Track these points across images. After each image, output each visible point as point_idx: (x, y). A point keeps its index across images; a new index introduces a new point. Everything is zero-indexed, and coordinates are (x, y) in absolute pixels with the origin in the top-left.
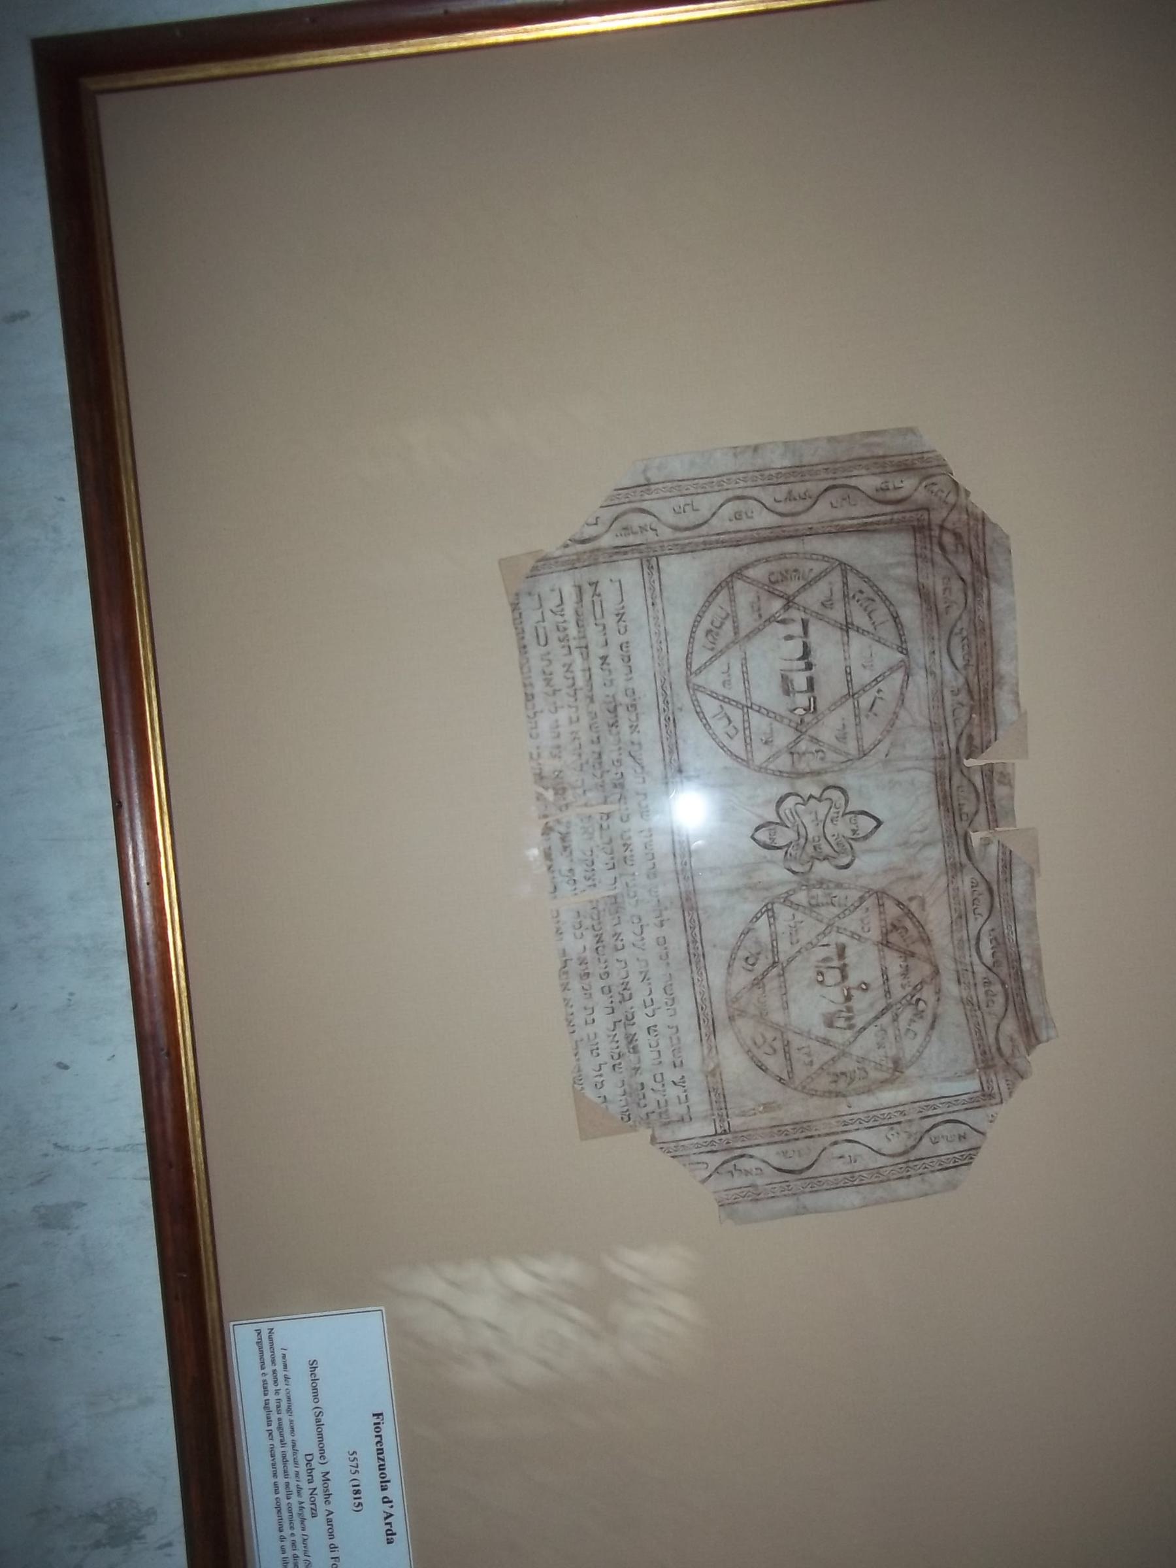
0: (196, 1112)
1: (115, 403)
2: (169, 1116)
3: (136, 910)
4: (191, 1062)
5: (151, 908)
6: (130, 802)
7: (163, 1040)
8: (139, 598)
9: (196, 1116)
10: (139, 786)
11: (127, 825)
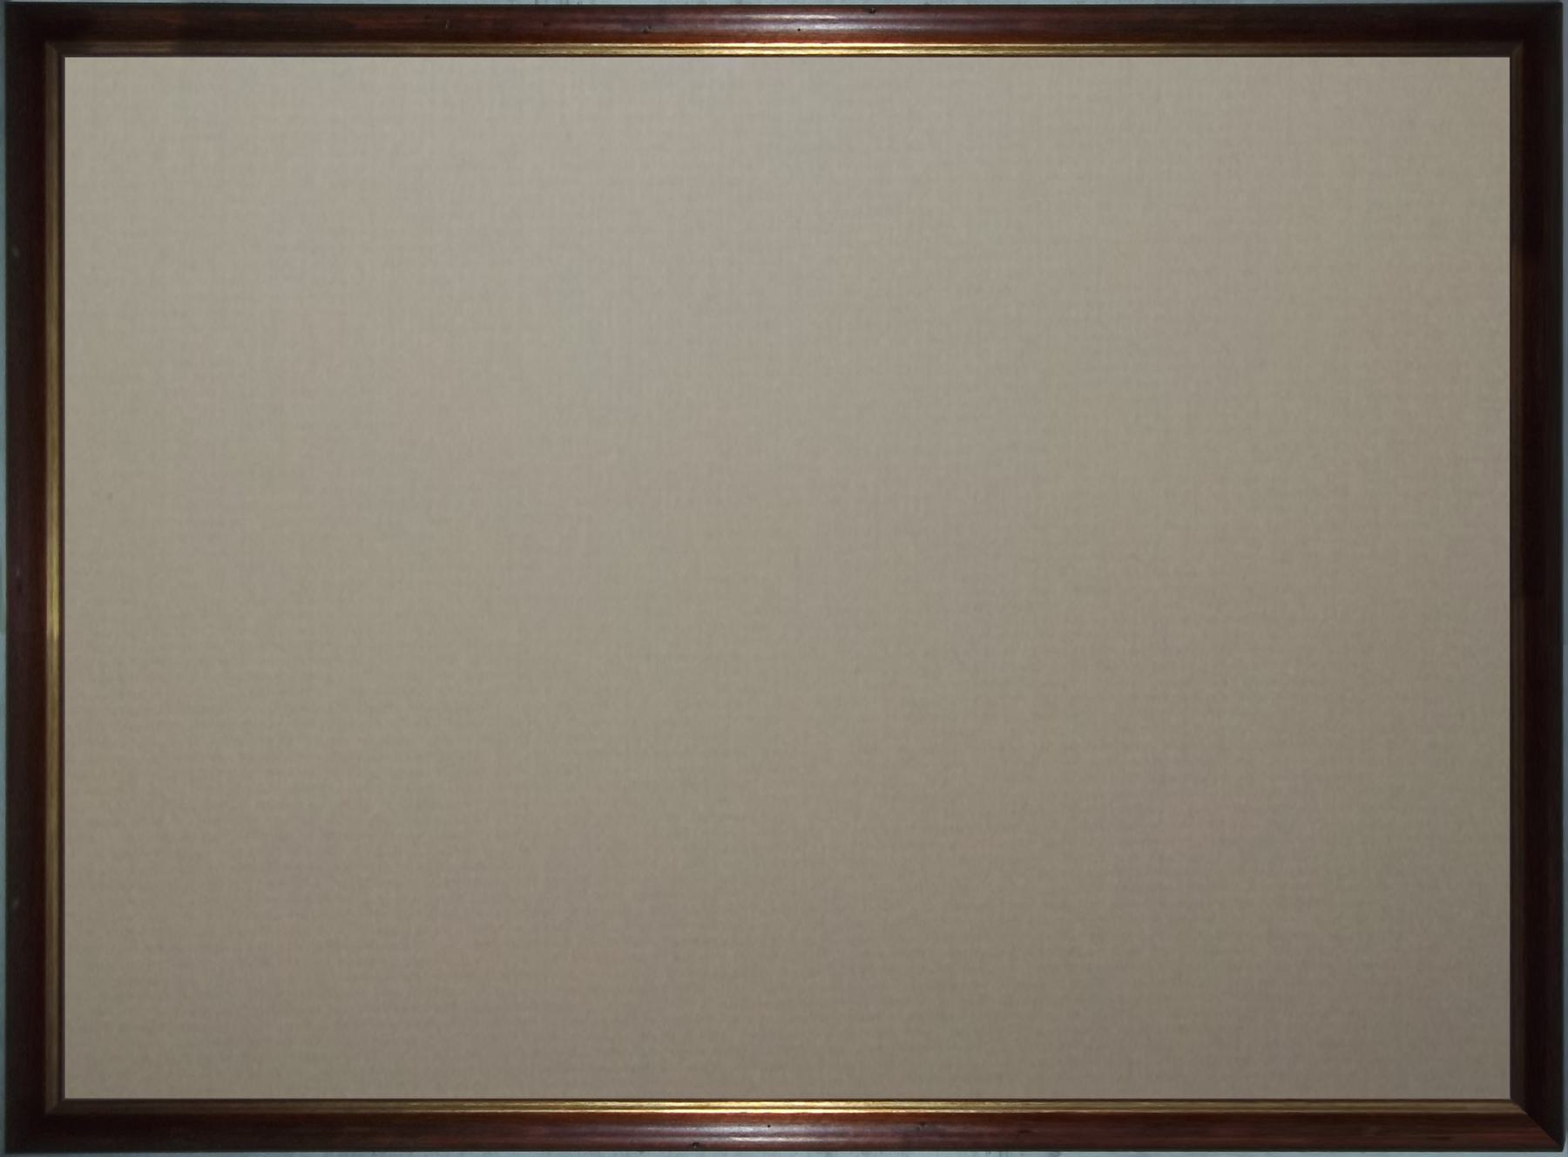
0: (592, 52)
1: (1230, 45)
2: (978, 1129)
3: (777, 16)
4: (932, 1104)
5: (791, 1126)
6: (695, 1135)
7: (658, 29)
8: (513, 1108)
9: (981, 1105)
10: (681, 1125)
11: (715, 1139)
